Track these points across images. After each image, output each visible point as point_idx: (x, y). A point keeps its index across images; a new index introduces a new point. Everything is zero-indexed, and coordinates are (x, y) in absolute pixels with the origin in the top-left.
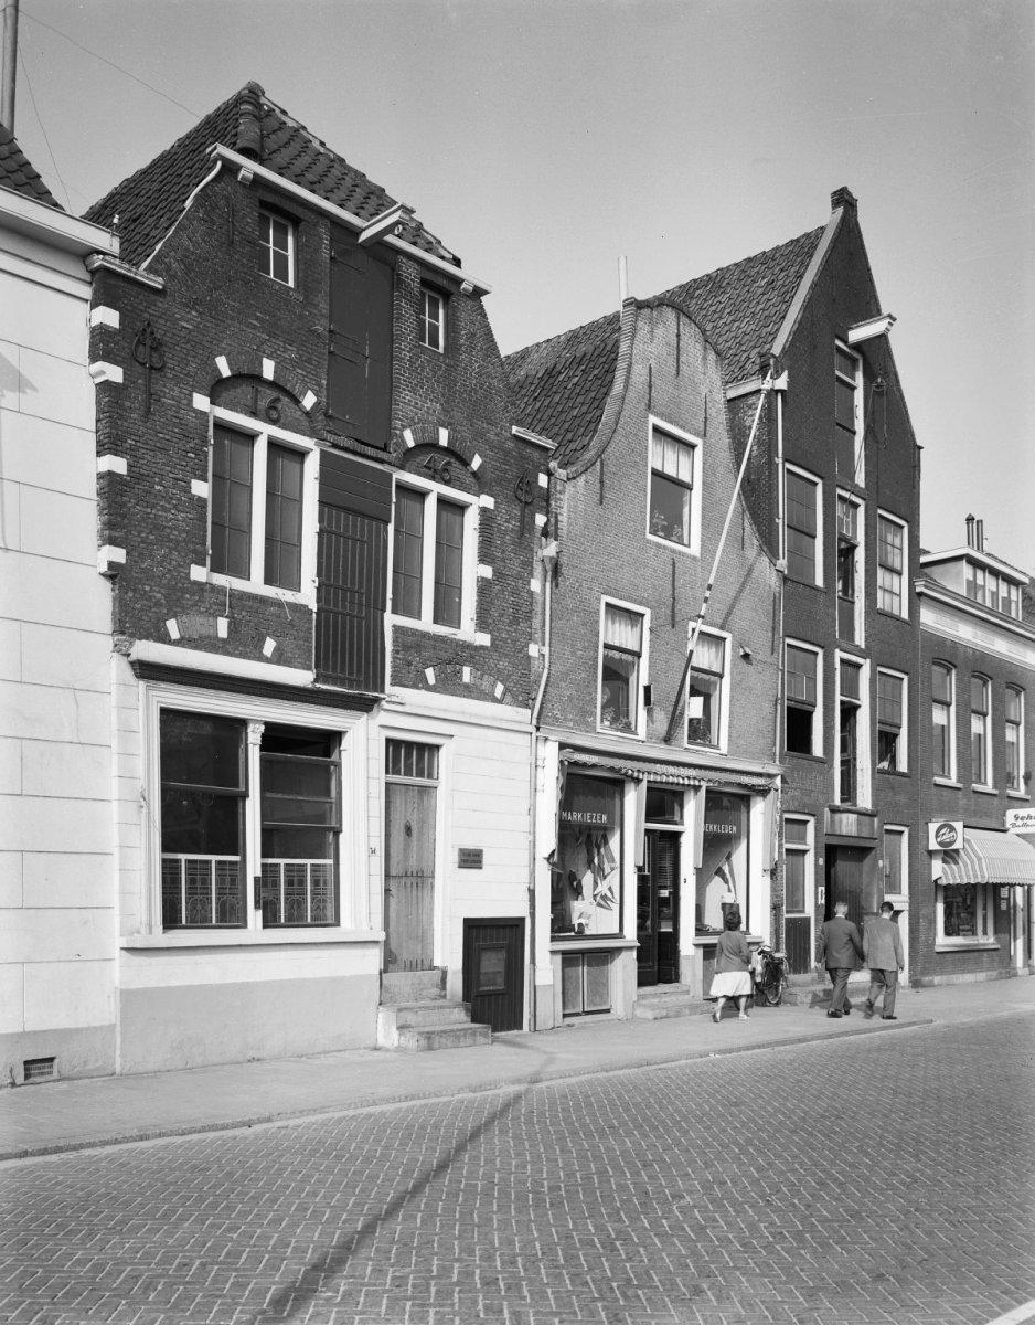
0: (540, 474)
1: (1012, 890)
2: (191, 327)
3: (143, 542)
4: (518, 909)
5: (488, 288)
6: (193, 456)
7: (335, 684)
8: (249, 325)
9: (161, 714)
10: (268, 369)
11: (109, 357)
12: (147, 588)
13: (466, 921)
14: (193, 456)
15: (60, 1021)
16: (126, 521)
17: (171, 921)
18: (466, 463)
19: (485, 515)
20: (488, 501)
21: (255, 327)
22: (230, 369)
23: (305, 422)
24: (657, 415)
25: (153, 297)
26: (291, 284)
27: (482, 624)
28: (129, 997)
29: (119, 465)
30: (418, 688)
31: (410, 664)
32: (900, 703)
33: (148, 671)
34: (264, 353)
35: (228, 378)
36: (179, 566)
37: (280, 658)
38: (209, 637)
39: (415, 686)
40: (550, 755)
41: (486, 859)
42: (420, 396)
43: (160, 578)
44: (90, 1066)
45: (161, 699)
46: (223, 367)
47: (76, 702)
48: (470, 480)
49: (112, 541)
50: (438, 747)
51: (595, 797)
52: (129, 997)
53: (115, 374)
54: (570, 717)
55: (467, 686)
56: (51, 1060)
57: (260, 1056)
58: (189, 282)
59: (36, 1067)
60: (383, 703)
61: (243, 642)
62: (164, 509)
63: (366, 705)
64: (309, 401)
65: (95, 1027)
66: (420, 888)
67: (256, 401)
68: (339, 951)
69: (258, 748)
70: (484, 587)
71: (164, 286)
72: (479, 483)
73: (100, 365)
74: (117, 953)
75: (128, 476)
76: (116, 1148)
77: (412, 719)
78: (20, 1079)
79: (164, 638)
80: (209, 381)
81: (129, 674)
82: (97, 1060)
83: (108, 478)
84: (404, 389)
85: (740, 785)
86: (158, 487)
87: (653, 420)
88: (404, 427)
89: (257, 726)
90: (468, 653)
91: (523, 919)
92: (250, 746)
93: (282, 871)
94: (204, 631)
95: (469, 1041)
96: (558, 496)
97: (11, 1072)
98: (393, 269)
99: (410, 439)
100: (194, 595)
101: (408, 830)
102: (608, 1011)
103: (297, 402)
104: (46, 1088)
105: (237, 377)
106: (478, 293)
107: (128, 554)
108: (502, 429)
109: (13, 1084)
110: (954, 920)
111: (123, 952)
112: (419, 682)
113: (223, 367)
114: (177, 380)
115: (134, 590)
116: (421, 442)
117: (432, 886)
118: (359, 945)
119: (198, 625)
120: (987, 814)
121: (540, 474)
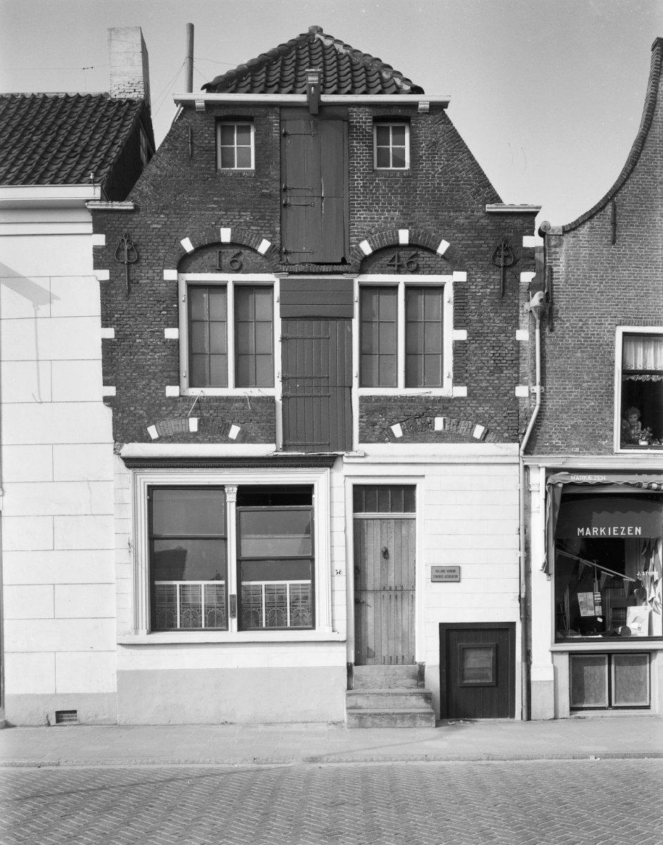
2: (159, 226)
3: (128, 379)
4: (510, 613)
5: (445, 99)
6: (165, 313)
7: (297, 450)
8: (207, 209)
10: (226, 235)
12: (132, 409)
13: (441, 625)
14: (165, 313)
15: (81, 689)
16: (115, 368)
17: (155, 627)
20: (461, 276)
21: (213, 209)
22: (193, 245)
23: (266, 264)
25: (129, 216)
27: (457, 381)
28: (123, 675)
30: (384, 442)
31: (374, 424)
33: (133, 463)
34: (222, 224)
35: (370, 256)
36: (157, 389)
37: (244, 438)
38: (183, 433)
39: (381, 440)
40: (538, 479)
41: (463, 575)
42: (376, 211)
43: (143, 400)
44: (100, 717)
46: (187, 245)
47: (89, 488)
50: (413, 487)
51: (639, 512)
52: (123, 675)
54: (574, 443)
55: (439, 433)
56: (75, 712)
57: (234, 721)
58: (158, 197)
59: (60, 716)
60: (345, 460)
61: (213, 429)
62: (143, 354)
63: (328, 462)
64: (264, 246)
65: (103, 694)
66: (399, 599)
67: (220, 261)
68: (238, 649)
69: (234, 505)
70: (459, 347)
71: (135, 206)
72: (451, 262)
74: (115, 647)
75: (115, 338)
76: (528, 762)
78: (53, 722)
79: (147, 439)
80: (177, 258)
81: (122, 464)
82: (104, 715)
84: (358, 211)
85: (627, 484)
86: (138, 341)
88: (360, 241)
90: (446, 406)
91: (514, 624)
93: (288, 591)
94: (178, 430)
95: (407, 723)
96: (553, 250)
97: (47, 717)
98: (346, 119)
99: (366, 248)
100: (169, 406)
101: (385, 554)
102: (648, 707)
104: (66, 730)
105: (200, 249)
106: (438, 108)
107: (117, 389)
108: (473, 212)
109: (49, 725)
111: (120, 647)
112: (389, 437)
113: (187, 245)
114: (150, 266)
115: (123, 412)
116: (378, 246)
117: (413, 597)
118: (325, 644)
119: (172, 426)
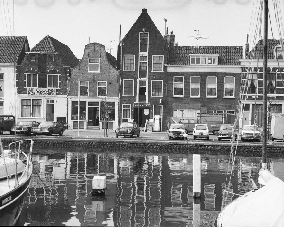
1: (104, 175)
11: (277, 97)
20: (60, 74)
46: (27, 70)
72: (58, 73)
110: (88, 125)
113: (27, 70)
120: (111, 128)
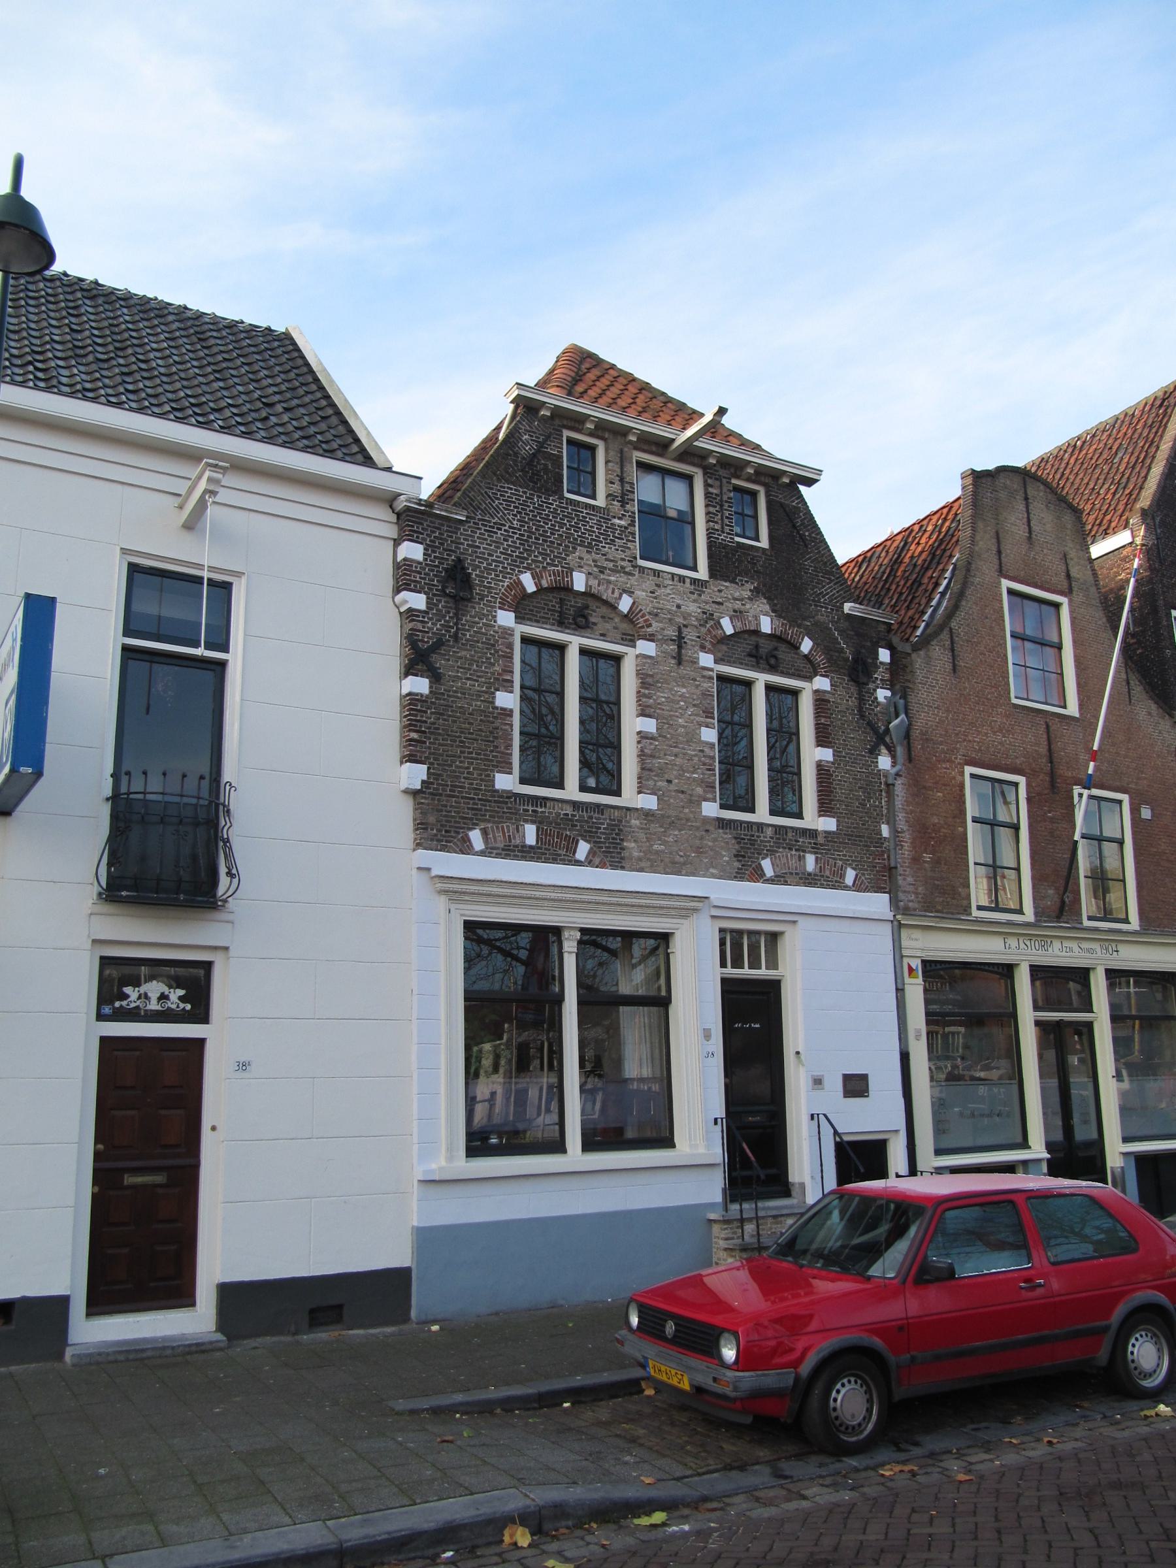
0: (881, 650)
9: (465, 927)
18: (796, 647)
19: (820, 701)
24: (1006, 577)
26: (764, 543)
27: (825, 808)
29: (420, 685)
32: (750, 767)
45: (462, 912)
48: (800, 663)
49: (412, 758)
53: (418, 601)
73: (405, 595)
77: (723, 910)
83: (412, 702)
87: (1006, 584)
89: (572, 933)
92: (566, 956)
103: (614, 608)
113: (529, 583)
121: (881, 650)
